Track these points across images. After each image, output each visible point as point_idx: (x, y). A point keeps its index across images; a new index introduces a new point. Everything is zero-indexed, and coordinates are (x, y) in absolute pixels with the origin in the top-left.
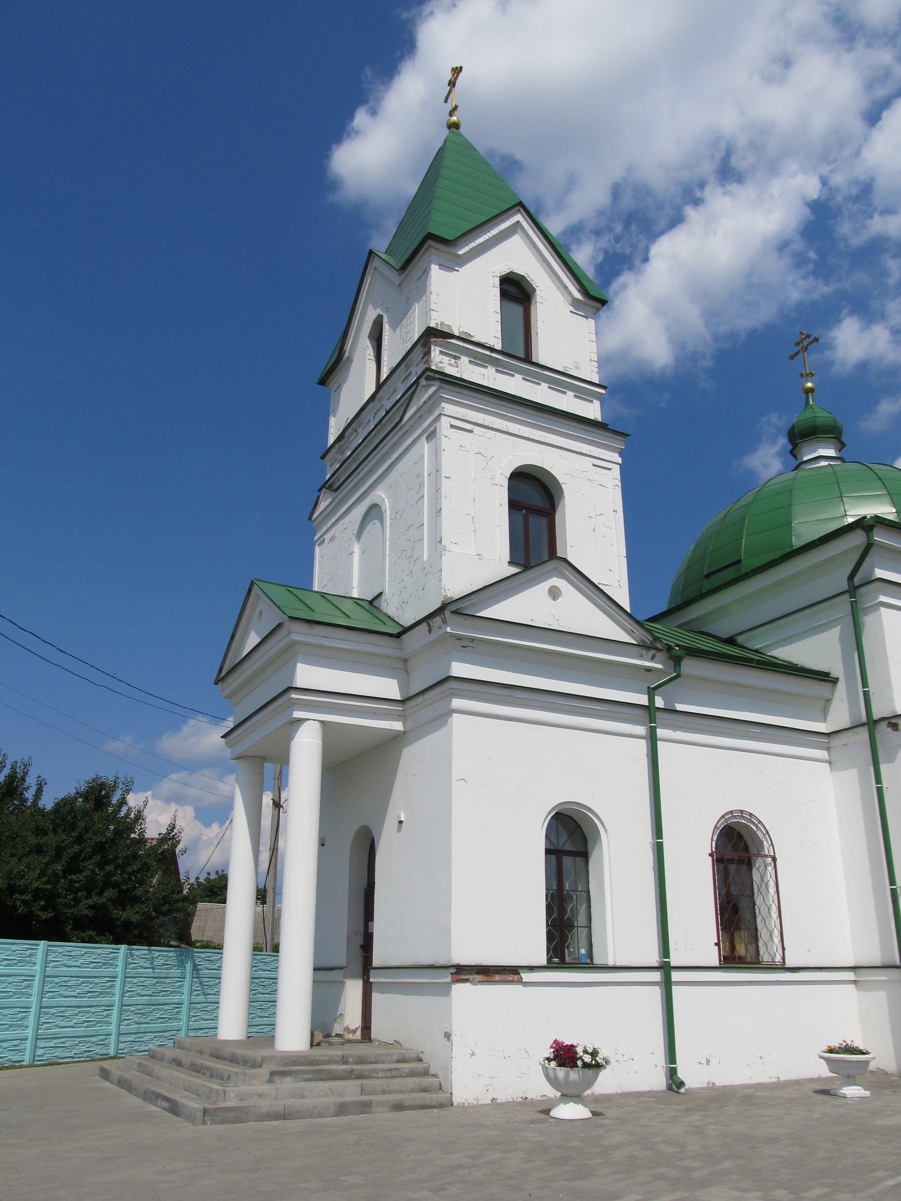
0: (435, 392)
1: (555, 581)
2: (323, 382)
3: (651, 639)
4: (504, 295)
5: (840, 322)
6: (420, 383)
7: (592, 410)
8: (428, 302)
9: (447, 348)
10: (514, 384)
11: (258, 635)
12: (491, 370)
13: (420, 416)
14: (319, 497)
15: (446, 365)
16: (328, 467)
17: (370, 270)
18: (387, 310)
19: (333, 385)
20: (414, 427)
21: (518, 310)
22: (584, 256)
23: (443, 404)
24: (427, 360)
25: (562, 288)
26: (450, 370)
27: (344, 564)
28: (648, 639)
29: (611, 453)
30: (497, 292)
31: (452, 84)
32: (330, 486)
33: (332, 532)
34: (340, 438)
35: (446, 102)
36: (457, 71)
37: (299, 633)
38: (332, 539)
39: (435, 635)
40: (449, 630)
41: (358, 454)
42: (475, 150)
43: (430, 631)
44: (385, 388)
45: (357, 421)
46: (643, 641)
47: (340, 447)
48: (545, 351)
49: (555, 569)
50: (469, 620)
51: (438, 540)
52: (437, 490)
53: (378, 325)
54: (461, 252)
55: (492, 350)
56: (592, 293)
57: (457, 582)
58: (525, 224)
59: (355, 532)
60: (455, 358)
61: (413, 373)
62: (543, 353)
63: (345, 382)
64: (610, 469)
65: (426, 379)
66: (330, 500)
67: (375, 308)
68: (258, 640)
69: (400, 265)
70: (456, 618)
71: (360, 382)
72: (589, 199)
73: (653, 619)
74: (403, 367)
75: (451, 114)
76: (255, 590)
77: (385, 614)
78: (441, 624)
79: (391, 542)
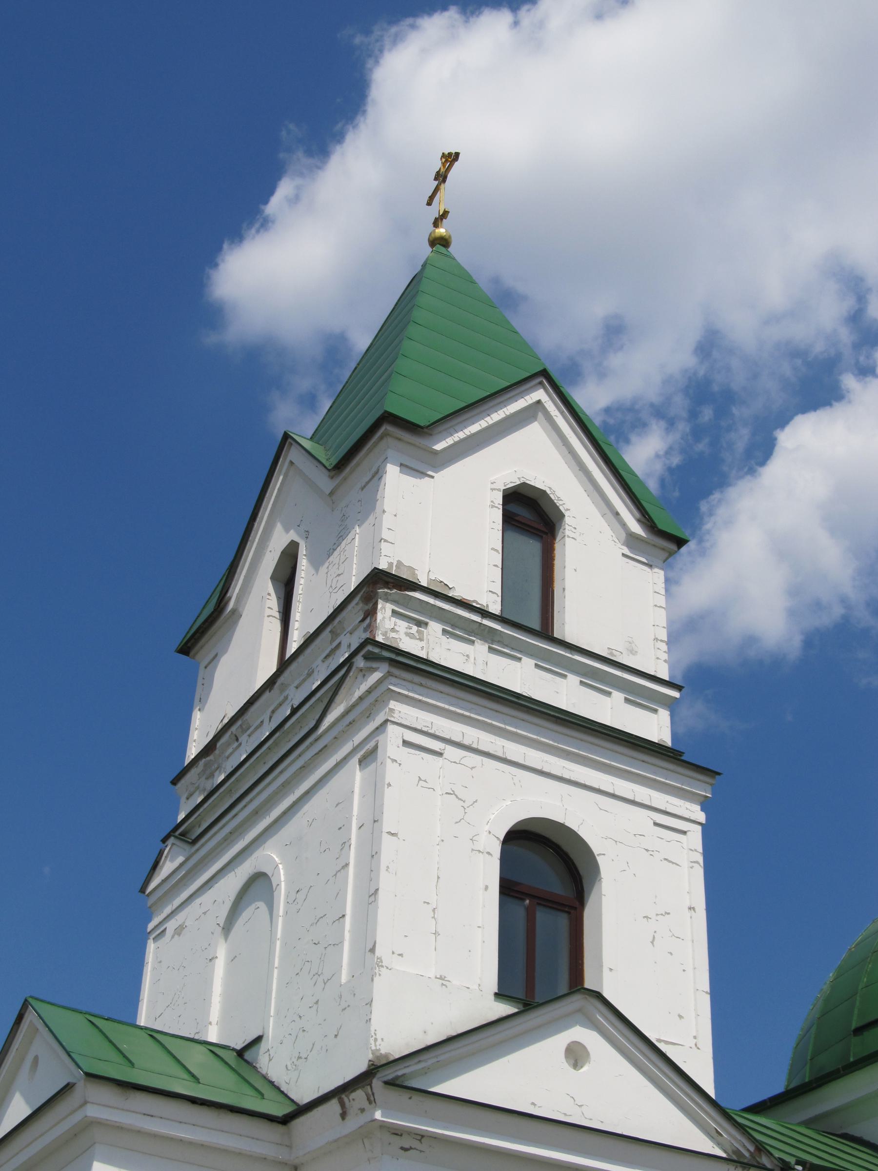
0: (380, 682)
1: (579, 1033)
2: (186, 649)
3: (752, 1148)
4: (510, 520)
5: (776, 439)
6: (356, 662)
7: (656, 727)
8: (377, 526)
9: (406, 606)
10: (520, 675)
11: (28, 1101)
12: (480, 648)
13: (350, 723)
14: (161, 853)
15: (402, 635)
16: (183, 799)
17: (283, 466)
18: (307, 535)
19: (203, 654)
20: (338, 741)
21: (532, 547)
22: (645, 454)
23: (393, 704)
24: (369, 625)
25: (610, 516)
26: (408, 645)
27: (198, 979)
28: (746, 1148)
29: (688, 805)
30: (498, 515)
31: (441, 177)
32: (183, 834)
33: (179, 918)
34: (208, 749)
35: (429, 203)
36: (451, 158)
37: (102, 1106)
38: (179, 930)
39: (354, 1123)
40: (378, 1115)
41: (237, 780)
42: (473, 282)
43: (343, 1115)
44: (294, 666)
45: (239, 723)
46: (737, 1152)
47: (206, 765)
48: (580, 617)
49: (580, 1010)
50: (417, 1098)
51: (369, 946)
52: (372, 856)
53: (290, 556)
54: (439, 447)
55: (484, 613)
56: (661, 526)
57: (400, 1024)
58: (552, 407)
59: (222, 921)
60: (419, 624)
61: (344, 647)
62: (572, 624)
63: (225, 650)
64: (684, 833)
65: (366, 658)
66: (181, 859)
67: (287, 530)
68: (26, 1112)
69: (334, 461)
70: (394, 1095)
71: (249, 655)
72: (642, 370)
73: (758, 1108)
74: (326, 633)
75: (436, 223)
76: (30, 1017)
77: (265, 1077)
78: (365, 1104)
79: (285, 945)
